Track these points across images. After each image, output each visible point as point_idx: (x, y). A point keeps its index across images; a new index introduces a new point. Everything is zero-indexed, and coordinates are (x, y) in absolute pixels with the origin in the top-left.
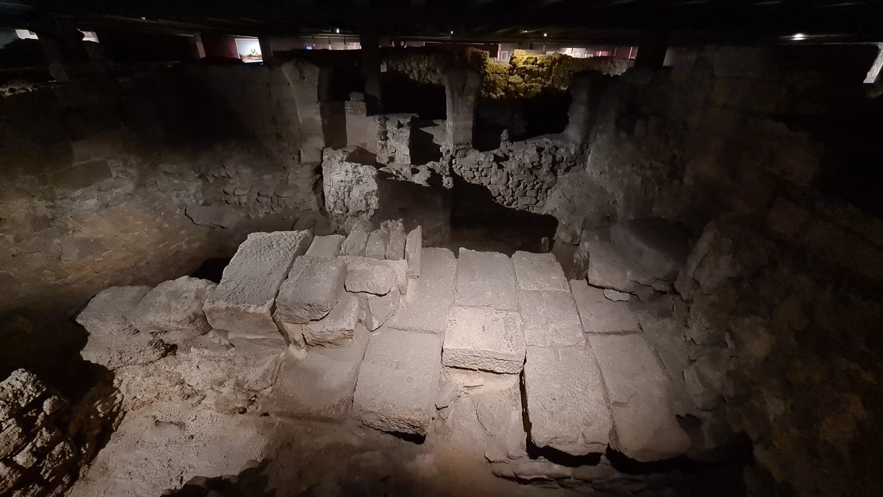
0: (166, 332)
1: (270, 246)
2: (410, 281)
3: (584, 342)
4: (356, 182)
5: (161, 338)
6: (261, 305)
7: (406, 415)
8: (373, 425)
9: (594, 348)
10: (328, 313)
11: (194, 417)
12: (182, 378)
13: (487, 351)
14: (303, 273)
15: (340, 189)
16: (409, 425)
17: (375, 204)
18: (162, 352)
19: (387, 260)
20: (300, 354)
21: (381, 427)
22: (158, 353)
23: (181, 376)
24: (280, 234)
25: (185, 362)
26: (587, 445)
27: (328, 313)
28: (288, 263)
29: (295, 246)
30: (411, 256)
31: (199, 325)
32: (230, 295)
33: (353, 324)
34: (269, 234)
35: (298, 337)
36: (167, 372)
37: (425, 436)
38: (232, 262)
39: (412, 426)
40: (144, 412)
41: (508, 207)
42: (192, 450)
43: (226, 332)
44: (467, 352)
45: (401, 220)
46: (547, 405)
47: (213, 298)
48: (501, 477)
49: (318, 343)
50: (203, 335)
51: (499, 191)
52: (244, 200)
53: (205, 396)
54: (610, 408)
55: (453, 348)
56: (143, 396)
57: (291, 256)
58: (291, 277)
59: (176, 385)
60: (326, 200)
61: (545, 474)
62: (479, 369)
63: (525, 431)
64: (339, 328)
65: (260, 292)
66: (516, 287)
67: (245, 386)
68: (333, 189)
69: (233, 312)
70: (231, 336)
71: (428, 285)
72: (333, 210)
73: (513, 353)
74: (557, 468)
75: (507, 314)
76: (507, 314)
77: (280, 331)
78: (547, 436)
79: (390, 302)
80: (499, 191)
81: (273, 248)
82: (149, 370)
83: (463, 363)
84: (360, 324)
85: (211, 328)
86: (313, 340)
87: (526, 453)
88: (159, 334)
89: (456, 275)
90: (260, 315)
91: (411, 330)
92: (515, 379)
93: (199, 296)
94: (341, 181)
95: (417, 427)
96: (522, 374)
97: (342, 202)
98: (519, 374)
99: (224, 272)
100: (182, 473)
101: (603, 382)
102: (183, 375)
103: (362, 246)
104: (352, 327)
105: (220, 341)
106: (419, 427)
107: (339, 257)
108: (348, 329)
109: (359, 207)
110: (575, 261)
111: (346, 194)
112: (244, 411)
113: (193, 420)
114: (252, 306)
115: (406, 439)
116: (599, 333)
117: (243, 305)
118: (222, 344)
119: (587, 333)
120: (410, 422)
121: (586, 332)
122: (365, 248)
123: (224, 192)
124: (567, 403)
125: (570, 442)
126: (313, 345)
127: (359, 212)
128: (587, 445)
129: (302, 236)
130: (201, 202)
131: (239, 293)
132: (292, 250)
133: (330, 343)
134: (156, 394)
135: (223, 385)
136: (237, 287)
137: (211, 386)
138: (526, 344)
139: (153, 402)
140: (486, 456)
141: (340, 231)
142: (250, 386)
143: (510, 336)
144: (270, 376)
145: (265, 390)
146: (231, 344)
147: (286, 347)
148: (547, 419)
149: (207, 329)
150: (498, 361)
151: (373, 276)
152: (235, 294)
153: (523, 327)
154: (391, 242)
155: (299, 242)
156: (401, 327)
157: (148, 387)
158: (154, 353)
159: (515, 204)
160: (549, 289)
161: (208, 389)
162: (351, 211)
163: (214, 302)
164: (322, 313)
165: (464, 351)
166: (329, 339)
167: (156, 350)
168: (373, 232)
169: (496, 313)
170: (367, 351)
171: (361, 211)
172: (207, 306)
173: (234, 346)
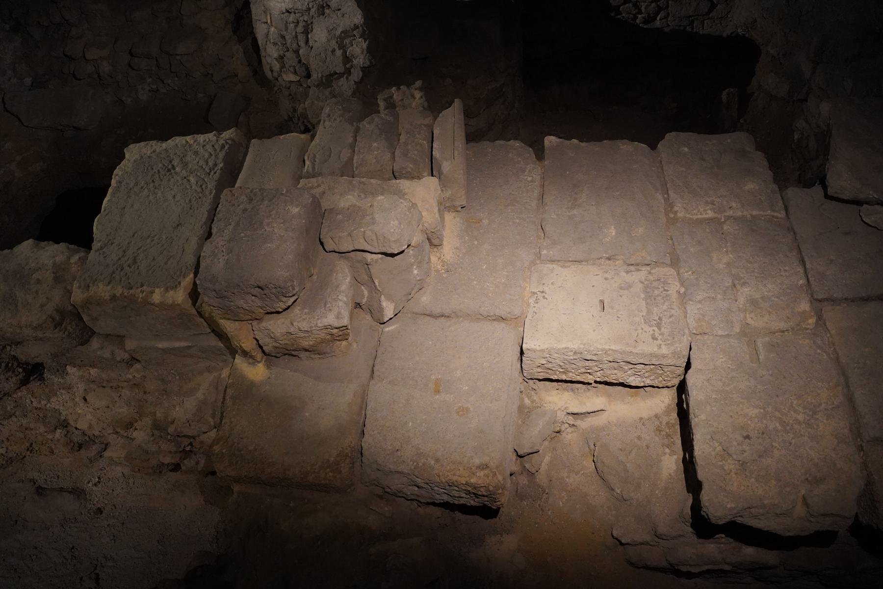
0: (19, 343)
1: (170, 170)
2: (449, 217)
3: (812, 321)
4: (318, 9)
5: (13, 353)
6: (172, 289)
7: (461, 477)
8: (403, 493)
9: (833, 332)
10: (297, 299)
11: (97, 480)
12: (63, 418)
13: (610, 349)
14: (238, 224)
15: (286, 29)
16: (468, 492)
17: (362, 57)
18: (21, 376)
19: (398, 181)
20: (256, 372)
21: (418, 496)
22: (14, 378)
23: (60, 414)
24: (184, 142)
25: (61, 391)
26: (811, 519)
27: (297, 299)
28: (209, 199)
29: (215, 165)
30: (446, 167)
31: (71, 330)
32: (114, 272)
33: (346, 314)
34: (164, 145)
35: (248, 344)
36: (36, 408)
37: (499, 508)
38: (105, 207)
39: (474, 494)
40: (16, 473)
41: (645, 27)
42: (103, 531)
43: (121, 338)
44: (571, 354)
45: (418, 83)
46: (733, 448)
47: (85, 279)
48: (644, 567)
49: (287, 352)
50: (82, 344)
52: (105, 68)
53: (107, 444)
54: (862, 450)
55: (542, 347)
56: (7, 449)
57: (211, 185)
58: (217, 233)
59: (56, 429)
60: (263, 54)
61: (728, 564)
62: (596, 382)
63: (688, 492)
64: (320, 325)
65: (166, 263)
66: (667, 214)
67: (171, 430)
68: (273, 29)
69: (125, 304)
70: (130, 345)
71: (486, 222)
72: (279, 75)
73: (664, 350)
74: (749, 552)
75: (650, 273)
76: (650, 273)
77: (213, 331)
78: (733, 506)
79: (412, 265)
81: (176, 173)
82: (7, 407)
83: (564, 373)
84: (359, 310)
85: (94, 333)
86: (276, 347)
87: (690, 529)
88: (8, 348)
89: (542, 197)
90: (173, 306)
91: (457, 316)
92: (666, 399)
93: (60, 276)
94: (288, 11)
95: (484, 496)
96: (682, 388)
98: (675, 388)
99: (94, 228)
100: (96, 569)
101: (850, 398)
102: (64, 413)
103: (345, 154)
104: (345, 321)
105: (113, 354)
106: (486, 496)
107: (303, 182)
108: (336, 324)
110: (796, 137)
111: (301, 38)
112: (176, 467)
113: (95, 485)
114: (157, 290)
115: (463, 513)
116: (846, 299)
118: (118, 359)
119: (820, 301)
120: (469, 489)
121: (817, 300)
122: (351, 159)
123: (66, 56)
124: (774, 444)
125: (778, 515)
126: (278, 355)
127: (331, 75)
128: (811, 519)
129: (227, 143)
130: (28, 81)
131: (129, 266)
132: (212, 173)
133: (307, 350)
134: (28, 445)
135: (133, 428)
136: (123, 256)
137: (114, 430)
138: (690, 331)
139: (25, 457)
140: (615, 535)
141: (299, 119)
142: (179, 430)
143: (657, 318)
144: (211, 412)
145: (206, 434)
146: (133, 358)
147: (230, 359)
148: (733, 474)
149: (86, 334)
150: (633, 366)
151: (373, 219)
152: (122, 270)
153: (684, 298)
154: (403, 138)
155: (221, 155)
156: (437, 310)
157: (12, 435)
158: (7, 379)
159: (661, 19)
160: (740, 214)
161: (109, 434)
162: (314, 76)
163: (88, 286)
164: (284, 299)
165: (564, 351)
166: (305, 343)
167: (10, 374)
168: (364, 123)
169: (627, 272)
170: (377, 361)
171: (336, 73)
172: (78, 296)
173: (139, 361)
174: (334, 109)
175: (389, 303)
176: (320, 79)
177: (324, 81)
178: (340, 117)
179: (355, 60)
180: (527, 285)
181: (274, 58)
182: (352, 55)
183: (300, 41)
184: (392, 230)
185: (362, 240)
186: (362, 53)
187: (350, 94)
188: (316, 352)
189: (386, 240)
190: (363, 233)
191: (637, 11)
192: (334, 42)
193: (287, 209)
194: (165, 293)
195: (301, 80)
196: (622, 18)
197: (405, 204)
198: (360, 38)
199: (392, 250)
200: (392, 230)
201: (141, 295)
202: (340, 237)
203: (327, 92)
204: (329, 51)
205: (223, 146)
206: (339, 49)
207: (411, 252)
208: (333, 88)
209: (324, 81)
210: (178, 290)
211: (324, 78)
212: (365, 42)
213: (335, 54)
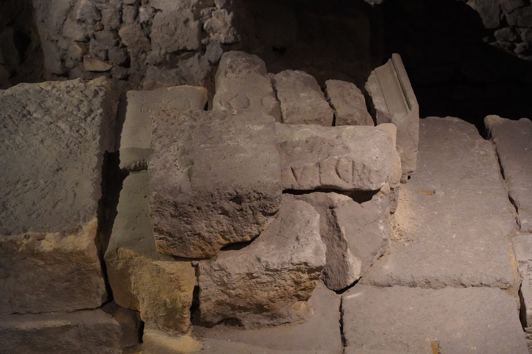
17: (224, 31)
29: (91, 111)
41: (526, 58)
51: (501, 12)
80: (501, 12)
97: (111, 35)
109: (180, 41)
117: (23, 235)
127: (177, 53)
132: (89, 119)
171: (185, 50)
174: (237, 60)
175: (356, 259)
176: (163, 57)
177: (168, 59)
178: (246, 68)
179: (214, 35)
180: (512, 255)
181: (76, 41)
182: (211, 28)
183: (125, 15)
184: (375, 158)
185: (333, 173)
186: (225, 25)
187: (203, 77)
188: (269, 314)
189: (365, 171)
190: (336, 162)
191: (515, 37)
192: (189, 11)
193: (247, 127)
194: (62, 238)
195: (114, 69)
196: (496, 45)
197: (383, 134)
198: (221, 8)
199: (370, 185)
200: (375, 158)
201: (25, 242)
202: (305, 168)
203: (173, 72)
204: (180, 21)
205: (96, 93)
206: (195, 20)
207: (380, 200)
208: (178, 69)
209: (168, 59)
210: (79, 234)
211: (168, 57)
212: (229, 14)
213: (188, 25)
